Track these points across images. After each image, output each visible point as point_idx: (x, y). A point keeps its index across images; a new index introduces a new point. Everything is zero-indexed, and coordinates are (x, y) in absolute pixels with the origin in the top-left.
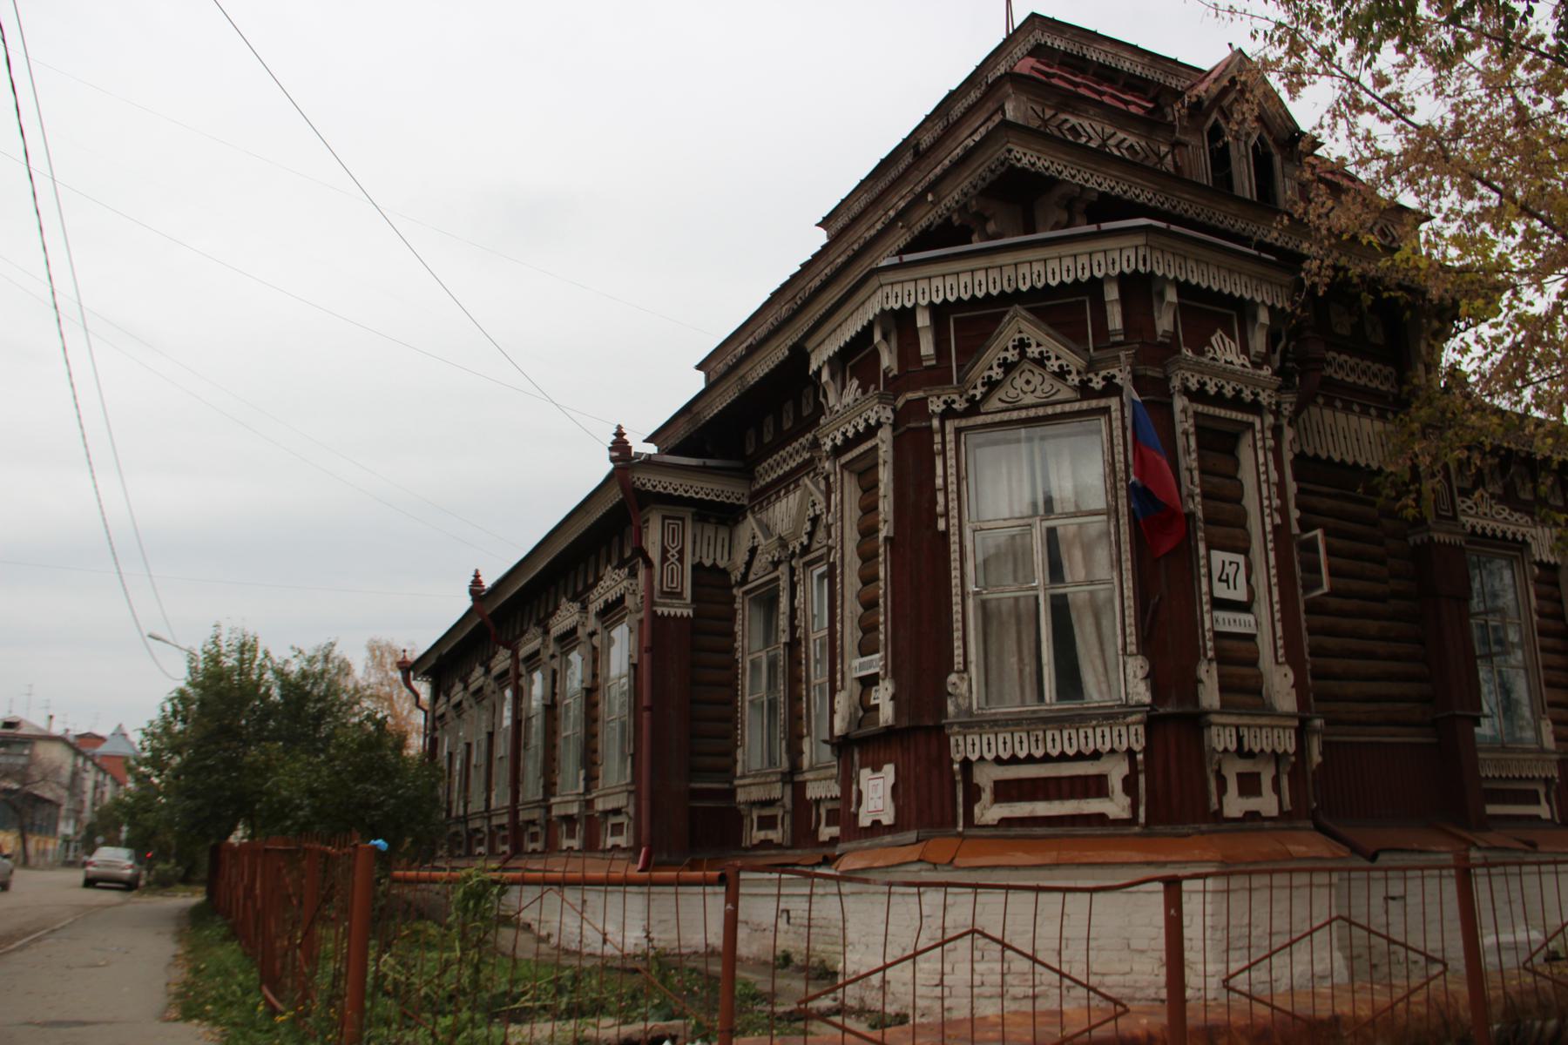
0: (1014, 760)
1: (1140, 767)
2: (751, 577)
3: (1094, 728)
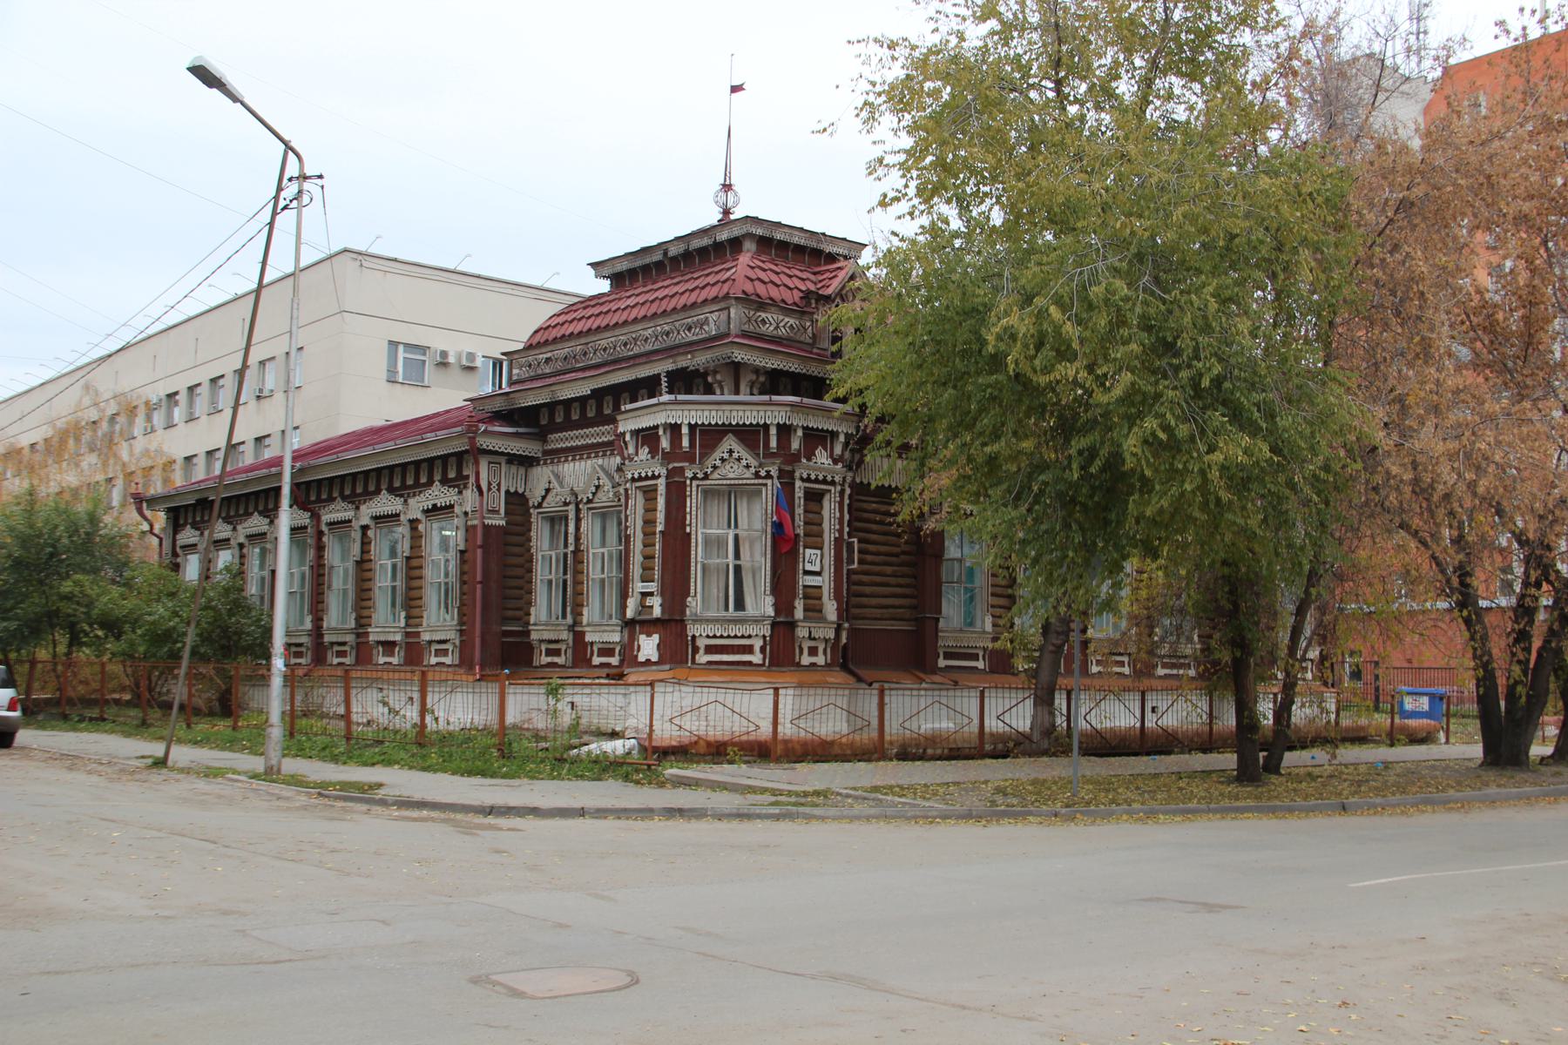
0: (715, 637)
2: (545, 505)
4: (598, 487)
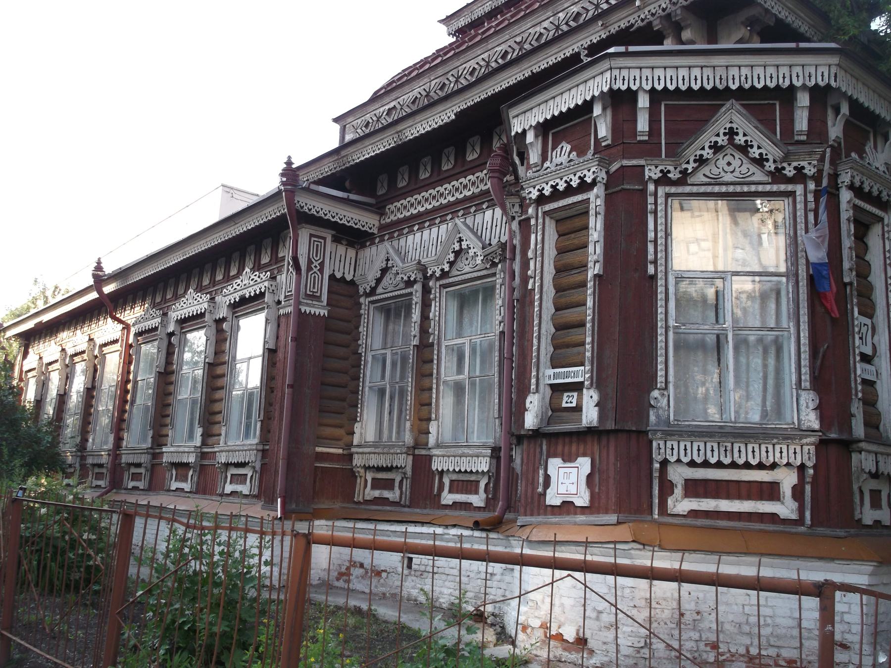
0: (706, 464)
1: (808, 480)
2: (380, 290)
3: (774, 445)
4: (457, 253)
